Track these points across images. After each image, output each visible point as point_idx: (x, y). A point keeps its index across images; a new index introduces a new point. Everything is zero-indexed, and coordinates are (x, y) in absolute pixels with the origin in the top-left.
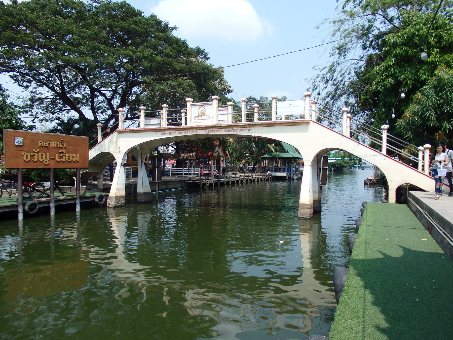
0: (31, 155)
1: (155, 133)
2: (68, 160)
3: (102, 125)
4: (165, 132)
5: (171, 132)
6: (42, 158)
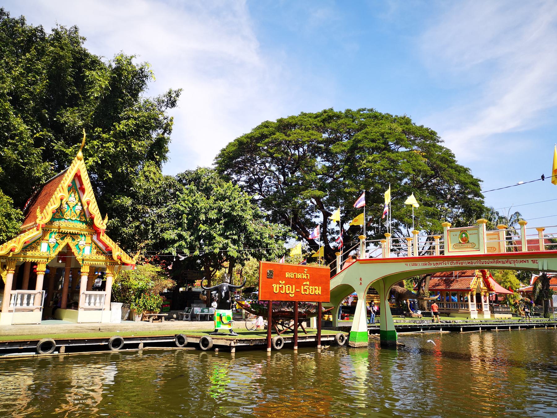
0: (279, 287)
1: (403, 264)
2: (311, 293)
3: (14, 272)
4: (416, 263)
5: (424, 262)
6: (289, 290)
